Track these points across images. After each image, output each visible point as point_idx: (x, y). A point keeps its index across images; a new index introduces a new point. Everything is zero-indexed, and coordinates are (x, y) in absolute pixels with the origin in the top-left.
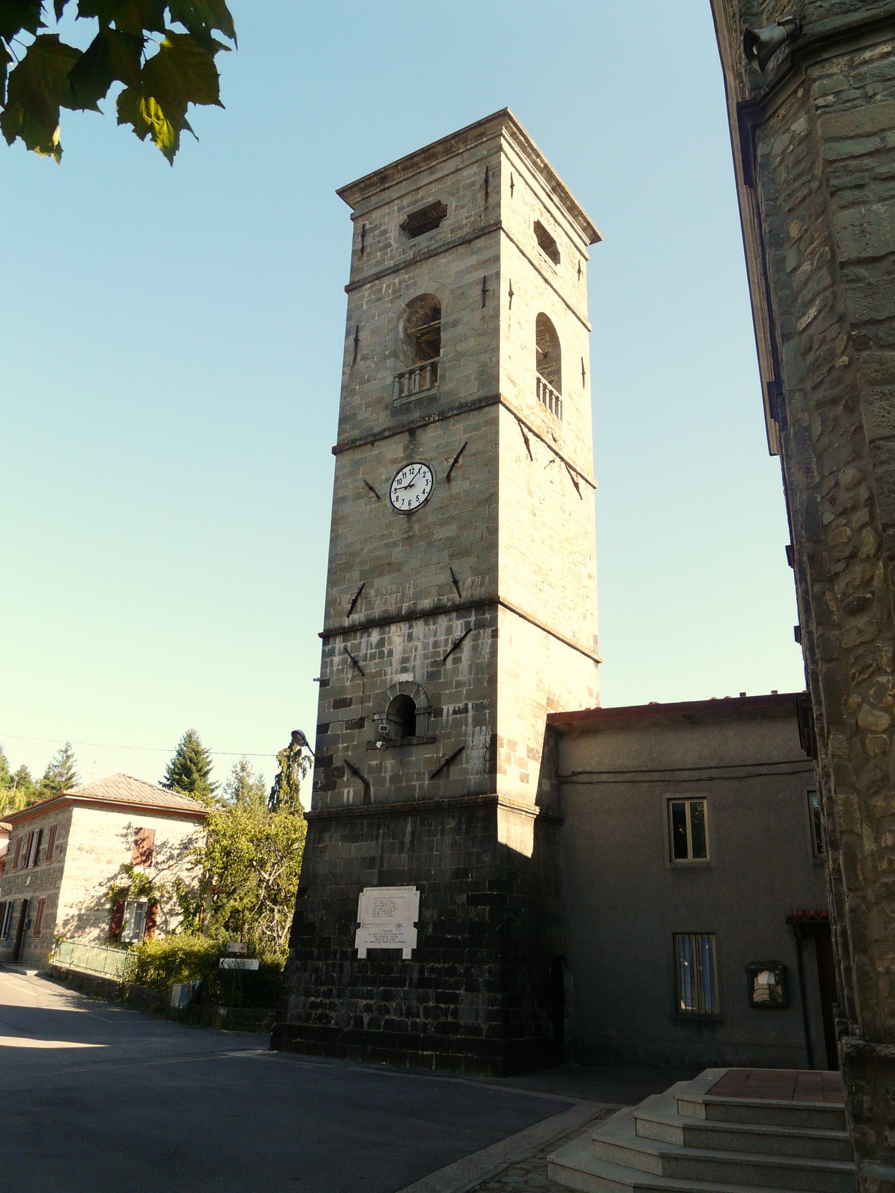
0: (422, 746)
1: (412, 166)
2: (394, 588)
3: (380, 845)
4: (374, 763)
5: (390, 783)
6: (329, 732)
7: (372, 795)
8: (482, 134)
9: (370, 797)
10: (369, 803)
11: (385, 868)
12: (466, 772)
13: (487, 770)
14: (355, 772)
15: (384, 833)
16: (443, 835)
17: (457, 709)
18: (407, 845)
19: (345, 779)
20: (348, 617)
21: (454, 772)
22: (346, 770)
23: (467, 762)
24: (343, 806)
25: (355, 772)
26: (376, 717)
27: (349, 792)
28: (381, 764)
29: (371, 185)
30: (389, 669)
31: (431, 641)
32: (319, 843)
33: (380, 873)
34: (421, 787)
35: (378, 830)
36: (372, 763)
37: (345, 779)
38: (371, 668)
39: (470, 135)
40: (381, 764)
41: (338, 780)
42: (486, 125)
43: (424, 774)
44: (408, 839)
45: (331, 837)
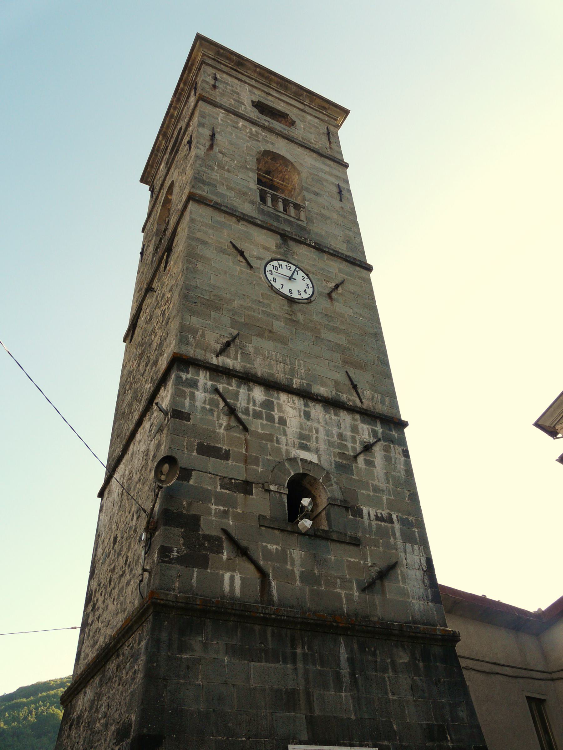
0: (343, 546)
1: (267, 78)
2: (280, 358)
3: (301, 671)
4: (273, 547)
5: (302, 581)
6: (191, 482)
7: (275, 592)
8: (325, 108)
9: (270, 594)
10: (270, 601)
11: (317, 713)
12: (404, 593)
13: (430, 597)
14: (243, 552)
15: (305, 655)
16: (395, 671)
17: (379, 515)
18: (346, 680)
19: (225, 556)
20: (217, 356)
21: (390, 587)
22: (225, 544)
23: (404, 582)
24: (223, 597)
25: (243, 552)
26: (272, 488)
27: (232, 578)
28: (284, 551)
29: (228, 58)
30: (283, 439)
31: (335, 430)
32: (181, 651)
33: (311, 721)
34: (349, 598)
35: (294, 647)
36: (269, 546)
37: (225, 556)
38: (257, 426)
39: (318, 100)
40: (284, 551)
41: (211, 555)
42: (331, 107)
43: (351, 582)
44: (345, 670)
45: (205, 646)
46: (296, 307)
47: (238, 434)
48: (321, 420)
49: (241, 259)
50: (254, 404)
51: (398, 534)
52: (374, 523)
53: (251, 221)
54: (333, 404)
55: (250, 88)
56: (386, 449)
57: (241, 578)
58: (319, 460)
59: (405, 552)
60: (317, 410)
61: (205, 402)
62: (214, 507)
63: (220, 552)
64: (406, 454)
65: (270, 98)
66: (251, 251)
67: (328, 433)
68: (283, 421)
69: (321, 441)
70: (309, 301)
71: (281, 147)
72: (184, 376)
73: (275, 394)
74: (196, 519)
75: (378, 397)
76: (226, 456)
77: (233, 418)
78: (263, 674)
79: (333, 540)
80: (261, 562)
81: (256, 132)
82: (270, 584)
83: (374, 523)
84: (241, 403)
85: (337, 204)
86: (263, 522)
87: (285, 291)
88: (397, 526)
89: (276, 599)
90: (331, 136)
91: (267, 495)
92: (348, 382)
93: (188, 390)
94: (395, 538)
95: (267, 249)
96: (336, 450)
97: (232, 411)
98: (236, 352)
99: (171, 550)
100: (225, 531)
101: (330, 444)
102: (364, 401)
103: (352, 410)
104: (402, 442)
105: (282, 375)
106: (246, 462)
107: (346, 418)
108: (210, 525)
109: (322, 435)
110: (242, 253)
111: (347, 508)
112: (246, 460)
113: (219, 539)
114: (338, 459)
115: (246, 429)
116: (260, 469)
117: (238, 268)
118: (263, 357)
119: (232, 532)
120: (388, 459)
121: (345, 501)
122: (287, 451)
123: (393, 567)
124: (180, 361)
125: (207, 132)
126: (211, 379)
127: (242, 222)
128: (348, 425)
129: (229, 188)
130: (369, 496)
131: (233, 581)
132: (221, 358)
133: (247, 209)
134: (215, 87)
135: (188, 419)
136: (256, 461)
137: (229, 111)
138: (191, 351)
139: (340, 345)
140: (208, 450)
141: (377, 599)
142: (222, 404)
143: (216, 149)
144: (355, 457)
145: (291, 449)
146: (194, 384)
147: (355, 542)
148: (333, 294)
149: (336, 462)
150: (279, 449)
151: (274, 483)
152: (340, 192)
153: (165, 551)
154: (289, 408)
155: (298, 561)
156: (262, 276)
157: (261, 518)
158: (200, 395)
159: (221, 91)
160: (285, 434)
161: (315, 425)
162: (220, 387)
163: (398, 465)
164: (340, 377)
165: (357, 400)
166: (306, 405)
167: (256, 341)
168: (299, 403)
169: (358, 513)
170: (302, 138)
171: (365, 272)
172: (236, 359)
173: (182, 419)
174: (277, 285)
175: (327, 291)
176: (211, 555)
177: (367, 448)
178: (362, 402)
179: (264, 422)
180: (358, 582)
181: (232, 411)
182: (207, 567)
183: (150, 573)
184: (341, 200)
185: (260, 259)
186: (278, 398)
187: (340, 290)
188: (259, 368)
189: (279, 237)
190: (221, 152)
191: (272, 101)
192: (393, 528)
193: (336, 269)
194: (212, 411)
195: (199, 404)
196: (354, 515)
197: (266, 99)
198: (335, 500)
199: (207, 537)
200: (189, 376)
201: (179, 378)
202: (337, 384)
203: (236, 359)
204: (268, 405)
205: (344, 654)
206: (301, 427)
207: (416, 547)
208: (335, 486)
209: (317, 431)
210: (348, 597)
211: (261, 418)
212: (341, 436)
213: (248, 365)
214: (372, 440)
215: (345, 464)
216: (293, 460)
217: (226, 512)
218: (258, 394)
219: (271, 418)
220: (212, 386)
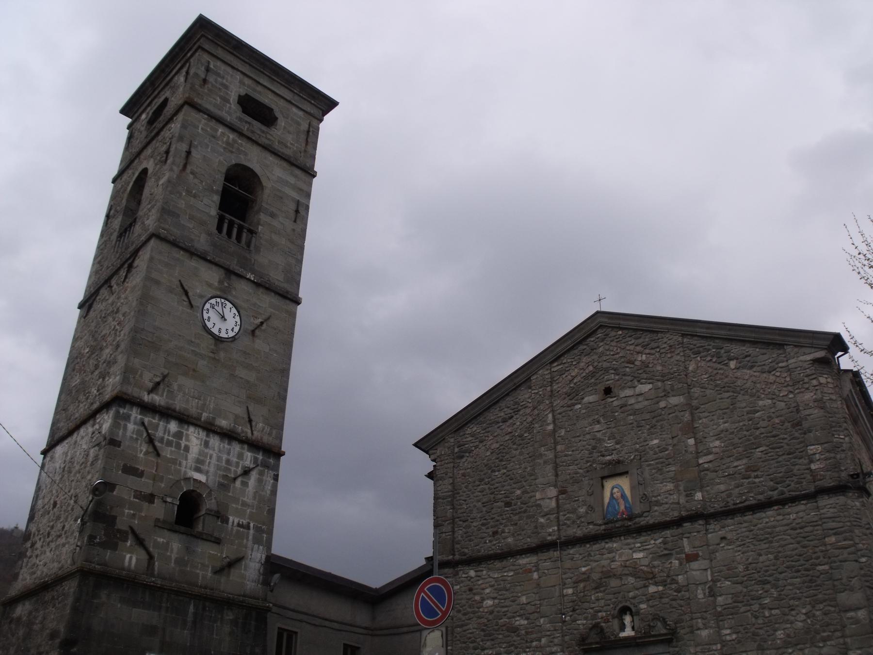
6: (115, 493)
7: (156, 569)
9: (153, 569)
10: (152, 575)
14: (140, 542)
21: (234, 573)
22: (130, 536)
23: (245, 569)
24: (123, 569)
25: (140, 542)
26: (169, 500)
27: (131, 558)
28: (168, 543)
30: (184, 462)
31: (225, 457)
36: (159, 539)
37: (129, 543)
38: (167, 452)
40: (168, 543)
41: (120, 543)
43: (208, 566)
46: (222, 346)
47: (152, 458)
48: (216, 448)
49: (185, 298)
50: (169, 435)
51: (251, 537)
52: (235, 528)
53: (203, 257)
54: (229, 436)
55: (242, 76)
56: (261, 474)
57: (137, 559)
58: (207, 480)
59: (252, 550)
60: (215, 441)
61: (133, 433)
62: (127, 511)
63: (127, 541)
64: (276, 478)
65: (259, 88)
66: (196, 289)
67: (219, 459)
68: (187, 449)
69: (212, 466)
70: (233, 338)
71: (255, 159)
72: (122, 411)
73: (186, 427)
74: (115, 518)
75: (267, 429)
76: (140, 474)
77: (151, 446)
78: (140, 616)
79: (203, 539)
80: (151, 549)
81: (233, 140)
82: (154, 564)
83: (235, 528)
84: (160, 433)
85: (289, 225)
86: (160, 525)
87: (215, 331)
88: (252, 532)
89: (156, 573)
90: (311, 137)
91: (164, 505)
92: (246, 416)
93: (122, 423)
94: (248, 540)
95: (210, 285)
96: (221, 473)
97: (151, 441)
98: (164, 390)
99: (95, 538)
100: (131, 528)
101: (218, 468)
102: (255, 433)
103: (242, 442)
104: (276, 468)
105: (194, 410)
106: (154, 480)
107: (236, 448)
108: (122, 524)
109: (214, 461)
110: (186, 293)
111: (218, 517)
112: (154, 478)
113: (126, 532)
114: (221, 480)
115: (158, 455)
116: (163, 485)
117: (181, 308)
118: (184, 395)
119: (136, 528)
120: (260, 481)
121: (218, 512)
122: (185, 472)
123: (239, 560)
124: (120, 400)
125: (184, 147)
126: (140, 414)
127: (194, 258)
128: (236, 452)
129: (192, 218)
130: (237, 508)
131: (131, 559)
132: (151, 395)
133: (202, 242)
134: (205, 81)
135: (119, 446)
136: (162, 479)
137: (212, 117)
138: (133, 391)
139: (248, 382)
140: (130, 470)
141: (223, 579)
142: (145, 435)
143: (189, 168)
144: (235, 479)
145: (188, 471)
146: (127, 418)
147: (218, 541)
148: (257, 332)
149: (219, 482)
150: (180, 471)
151: (170, 497)
152: (297, 211)
153: (92, 538)
154: (194, 438)
155: (175, 550)
156: (199, 315)
157: (157, 520)
158: (131, 426)
159: (210, 86)
160: (186, 459)
161: (211, 452)
162: (146, 420)
163: (266, 487)
164: (240, 411)
165: (249, 431)
166: (207, 436)
167: (182, 380)
168: (203, 434)
169: (226, 520)
170: (279, 142)
171: (294, 305)
172: (162, 396)
173: (115, 446)
174: (209, 325)
175: (251, 328)
176: (120, 543)
177: (246, 472)
178: (252, 434)
179: (173, 449)
180: (213, 567)
181: (151, 441)
182: (116, 550)
183: (81, 548)
184: (295, 221)
185: (201, 296)
186: (187, 430)
187: (264, 327)
188: (179, 404)
189: (222, 272)
190: (192, 173)
191: (260, 93)
192: (248, 533)
193: (266, 302)
194: (137, 439)
195: (129, 434)
196: (222, 522)
197: (254, 90)
198: (211, 511)
199: (119, 531)
200: (125, 411)
201: (118, 412)
202: (237, 417)
203: (162, 396)
204: (179, 435)
205: (191, 609)
206: (200, 454)
207: (261, 547)
208: (213, 501)
209: (211, 457)
210: (204, 575)
211: (171, 446)
212: (228, 462)
213: (171, 402)
214: (252, 466)
215: (225, 484)
216: (188, 479)
217: (134, 515)
218: (173, 426)
219: (178, 446)
220: (141, 419)
